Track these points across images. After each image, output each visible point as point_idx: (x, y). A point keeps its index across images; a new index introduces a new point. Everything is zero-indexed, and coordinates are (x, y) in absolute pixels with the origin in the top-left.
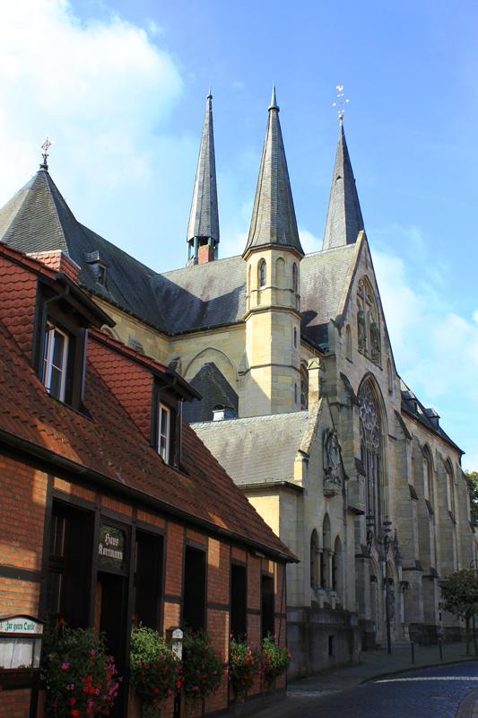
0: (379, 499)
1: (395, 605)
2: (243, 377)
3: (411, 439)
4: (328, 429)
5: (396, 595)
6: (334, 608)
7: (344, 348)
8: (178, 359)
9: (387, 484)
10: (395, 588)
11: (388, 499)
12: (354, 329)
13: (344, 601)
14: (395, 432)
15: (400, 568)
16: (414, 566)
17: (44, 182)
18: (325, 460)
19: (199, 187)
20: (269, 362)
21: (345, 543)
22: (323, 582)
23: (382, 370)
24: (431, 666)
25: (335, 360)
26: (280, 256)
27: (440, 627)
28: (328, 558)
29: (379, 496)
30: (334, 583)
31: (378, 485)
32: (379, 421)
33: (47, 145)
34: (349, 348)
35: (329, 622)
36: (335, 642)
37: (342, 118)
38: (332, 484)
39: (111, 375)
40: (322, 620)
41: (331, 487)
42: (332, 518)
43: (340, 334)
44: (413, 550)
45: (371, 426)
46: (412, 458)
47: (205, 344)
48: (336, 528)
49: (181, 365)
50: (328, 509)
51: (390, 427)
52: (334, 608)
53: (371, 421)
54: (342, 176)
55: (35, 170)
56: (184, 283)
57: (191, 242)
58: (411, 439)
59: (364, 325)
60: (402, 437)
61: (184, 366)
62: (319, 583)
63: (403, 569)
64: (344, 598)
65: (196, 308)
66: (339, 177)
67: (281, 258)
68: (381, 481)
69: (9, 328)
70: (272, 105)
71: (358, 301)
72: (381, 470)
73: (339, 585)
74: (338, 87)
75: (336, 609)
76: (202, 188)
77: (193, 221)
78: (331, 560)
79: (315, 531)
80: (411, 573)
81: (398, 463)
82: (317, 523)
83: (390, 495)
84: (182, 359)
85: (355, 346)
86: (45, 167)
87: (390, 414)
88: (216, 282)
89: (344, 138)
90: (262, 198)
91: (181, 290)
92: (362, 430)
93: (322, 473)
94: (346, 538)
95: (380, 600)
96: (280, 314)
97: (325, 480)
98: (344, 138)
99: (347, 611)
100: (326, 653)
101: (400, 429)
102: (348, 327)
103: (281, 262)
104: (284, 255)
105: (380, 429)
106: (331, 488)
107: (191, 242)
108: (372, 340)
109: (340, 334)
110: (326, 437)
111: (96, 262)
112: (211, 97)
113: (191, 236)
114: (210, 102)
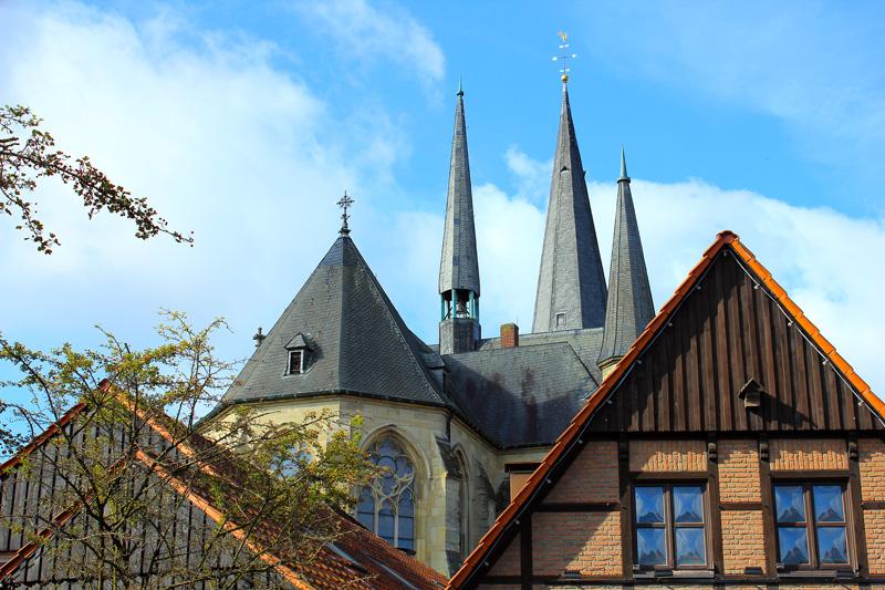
17: (347, 256)
19: (455, 220)
20: (335, 385)
33: (345, 202)
37: (565, 80)
54: (570, 167)
56: (490, 371)
57: (446, 296)
65: (521, 412)
66: (565, 169)
69: (171, 410)
70: (621, 176)
74: (560, 33)
76: (457, 221)
77: (449, 266)
86: (345, 231)
88: (537, 378)
89: (569, 110)
90: (621, 294)
91: (489, 383)
98: (569, 110)
107: (446, 296)
111: (441, 368)
112: (461, 94)
113: (448, 286)
114: (462, 101)
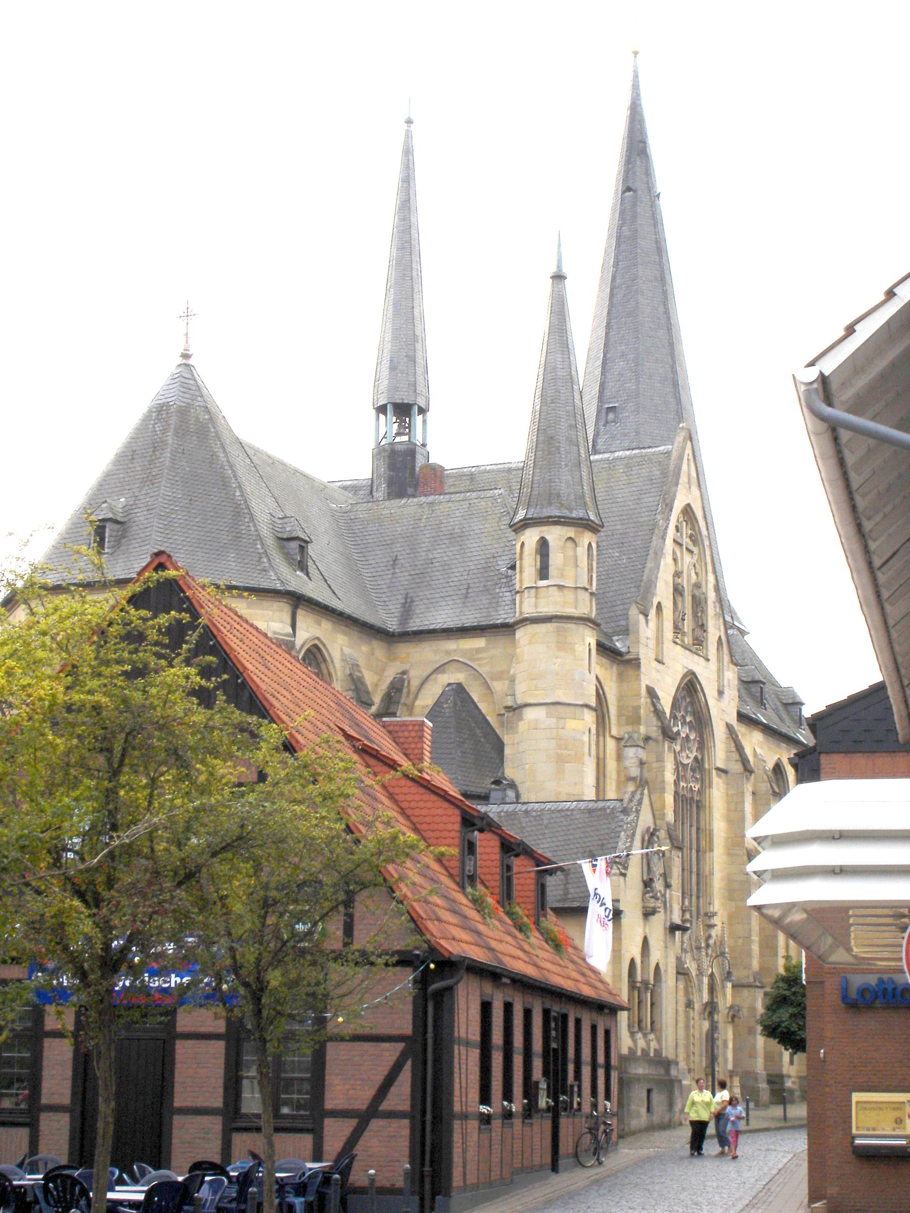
0: (698, 875)
1: (720, 1043)
2: (511, 714)
3: (751, 772)
4: (649, 828)
5: (721, 1025)
6: (652, 1054)
7: (652, 643)
8: (404, 673)
9: (711, 850)
10: (720, 1017)
11: (712, 873)
12: (668, 606)
13: (664, 1046)
14: (728, 759)
15: (729, 985)
16: (751, 980)
18: (645, 869)
21: (666, 971)
22: (640, 1021)
23: (708, 660)
24: (683, 883)
25: (638, 666)
26: (573, 535)
27: (789, 1077)
28: (646, 993)
29: (698, 869)
30: (652, 1023)
31: (698, 851)
32: (702, 746)
34: (659, 640)
35: (647, 1072)
36: (655, 1096)
38: (653, 900)
39: (418, 802)
40: (640, 1070)
41: (652, 903)
42: (652, 942)
43: (647, 621)
44: (749, 954)
45: (688, 758)
46: (753, 793)
47: (448, 653)
48: (656, 955)
49: (409, 682)
50: (647, 931)
51: (720, 753)
52: (652, 1054)
53: (689, 749)
55: (171, 364)
58: (751, 772)
59: (682, 595)
60: (737, 767)
61: (415, 683)
62: (649, 1026)
63: (733, 986)
64: (664, 1043)
67: (570, 538)
68: (703, 843)
71: (674, 553)
72: (702, 826)
73: (657, 1026)
75: (655, 1056)
78: (649, 994)
79: (632, 961)
80: (745, 992)
81: (729, 810)
82: (633, 950)
83: (716, 868)
84: (412, 673)
85: (669, 634)
87: (719, 731)
92: (678, 764)
93: (640, 886)
94: (667, 967)
95: (697, 1036)
96: (569, 625)
97: (644, 894)
99: (666, 1058)
100: (643, 1110)
101: (736, 756)
102: (659, 606)
103: (570, 544)
104: (576, 532)
105: (703, 759)
106: (652, 905)
107: (382, 409)
108: (695, 614)
109: (647, 621)
110: (646, 838)
